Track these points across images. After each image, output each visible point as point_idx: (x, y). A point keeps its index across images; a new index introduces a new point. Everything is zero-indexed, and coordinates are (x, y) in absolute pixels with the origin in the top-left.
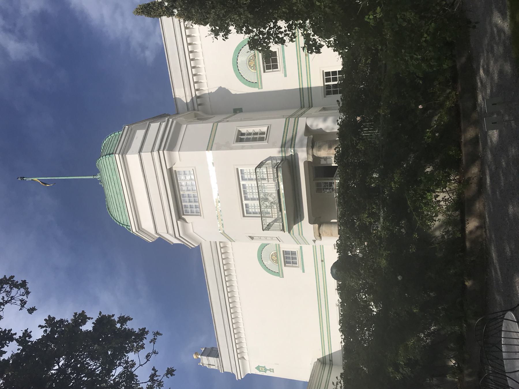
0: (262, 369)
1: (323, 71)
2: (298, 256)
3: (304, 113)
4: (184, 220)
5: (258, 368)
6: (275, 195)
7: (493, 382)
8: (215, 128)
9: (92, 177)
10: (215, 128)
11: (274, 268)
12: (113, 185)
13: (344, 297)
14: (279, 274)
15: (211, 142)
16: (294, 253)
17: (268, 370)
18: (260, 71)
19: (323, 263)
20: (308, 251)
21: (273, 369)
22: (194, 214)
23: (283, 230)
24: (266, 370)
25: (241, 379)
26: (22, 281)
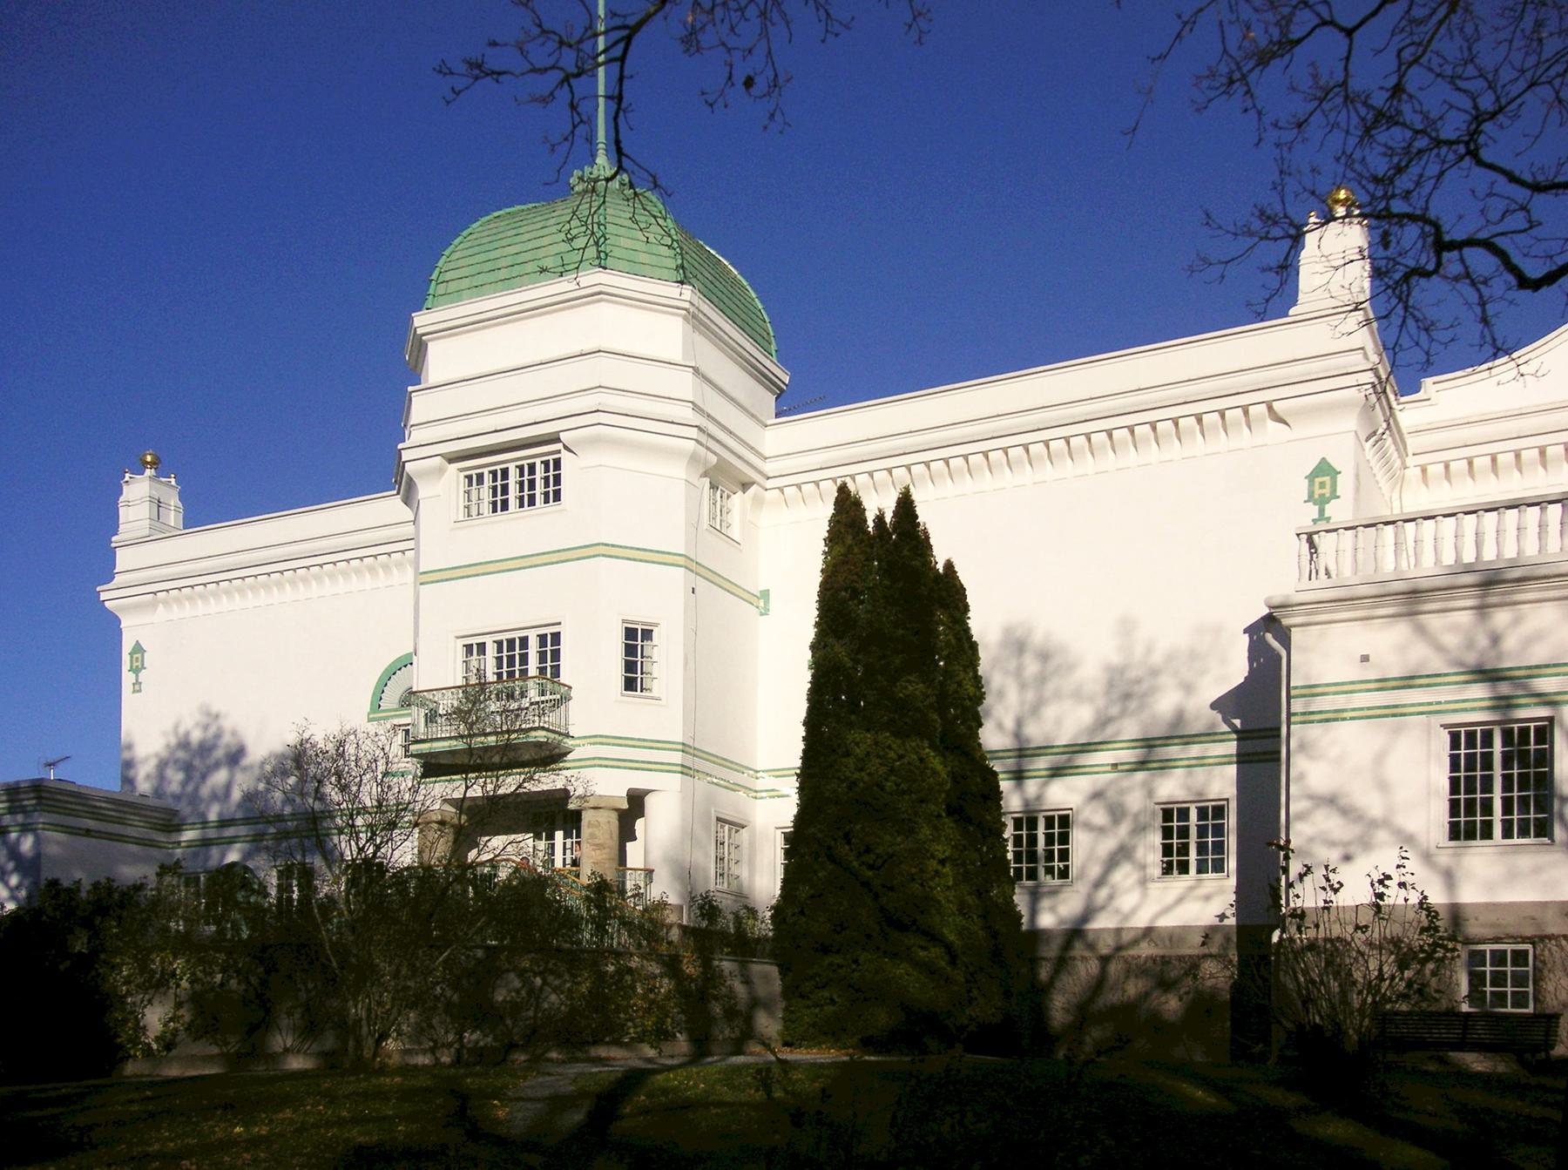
0: (1322, 485)
1: (656, 625)
3: (255, 820)
5: (138, 649)
13: (506, 927)
17: (137, 676)
19: (1109, 768)
21: (140, 691)
22: (1213, 803)
24: (136, 671)
25: (102, 599)
26: (906, 506)
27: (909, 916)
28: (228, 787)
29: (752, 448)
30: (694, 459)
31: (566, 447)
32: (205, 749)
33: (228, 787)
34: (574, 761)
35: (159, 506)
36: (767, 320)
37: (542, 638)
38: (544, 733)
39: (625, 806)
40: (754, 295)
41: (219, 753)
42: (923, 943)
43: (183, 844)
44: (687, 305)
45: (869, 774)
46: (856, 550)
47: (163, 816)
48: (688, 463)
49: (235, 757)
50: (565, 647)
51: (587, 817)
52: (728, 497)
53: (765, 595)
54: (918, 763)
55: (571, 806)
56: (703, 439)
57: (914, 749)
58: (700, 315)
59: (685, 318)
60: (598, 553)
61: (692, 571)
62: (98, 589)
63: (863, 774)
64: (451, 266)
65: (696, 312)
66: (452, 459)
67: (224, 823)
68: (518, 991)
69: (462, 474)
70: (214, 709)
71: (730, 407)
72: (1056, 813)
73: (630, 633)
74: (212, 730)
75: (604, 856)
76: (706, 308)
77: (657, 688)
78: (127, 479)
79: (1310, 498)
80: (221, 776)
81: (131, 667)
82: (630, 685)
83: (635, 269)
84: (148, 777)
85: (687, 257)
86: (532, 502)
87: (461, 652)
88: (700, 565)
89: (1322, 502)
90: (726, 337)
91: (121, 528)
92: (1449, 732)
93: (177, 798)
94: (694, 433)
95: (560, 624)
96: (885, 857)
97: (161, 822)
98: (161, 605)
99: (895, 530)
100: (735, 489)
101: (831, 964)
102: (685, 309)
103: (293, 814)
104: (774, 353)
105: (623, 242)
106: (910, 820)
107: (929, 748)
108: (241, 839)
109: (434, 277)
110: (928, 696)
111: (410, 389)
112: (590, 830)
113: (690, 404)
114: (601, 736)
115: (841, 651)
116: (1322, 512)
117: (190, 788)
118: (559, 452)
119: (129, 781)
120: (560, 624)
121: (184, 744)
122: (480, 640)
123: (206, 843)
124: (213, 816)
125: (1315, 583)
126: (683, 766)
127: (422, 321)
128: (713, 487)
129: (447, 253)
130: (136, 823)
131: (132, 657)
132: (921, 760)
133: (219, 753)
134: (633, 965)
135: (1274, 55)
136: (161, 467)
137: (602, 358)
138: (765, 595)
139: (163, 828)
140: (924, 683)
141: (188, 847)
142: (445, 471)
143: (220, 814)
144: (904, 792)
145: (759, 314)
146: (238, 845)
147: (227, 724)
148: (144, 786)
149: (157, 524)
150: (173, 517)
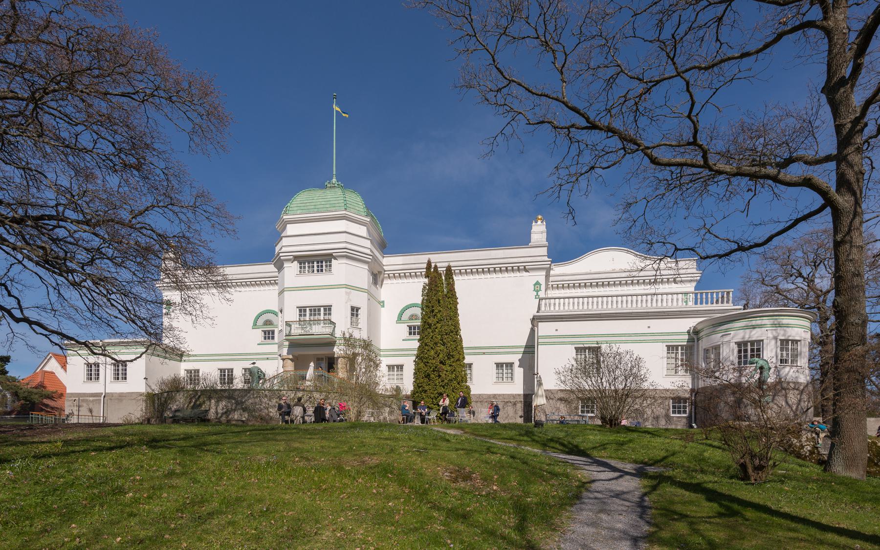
0: (537, 287)
2: (270, 341)
4: (294, 261)
6: (311, 332)
7: (115, 288)
8: (363, 290)
9: (334, 173)
10: (363, 290)
11: (261, 322)
12: (323, 203)
14: (255, 325)
15: (352, 288)
16: (273, 338)
18: (409, 323)
20: (274, 348)
23: (286, 336)
53: (383, 302)
72: (761, 353)
79: (534, 290)
86: (322, 271)
89: (537, 291)
92: (575, 348)
116: (537, 294)
125: (697, 306)
135: (813, 162)
138: (383, 302)
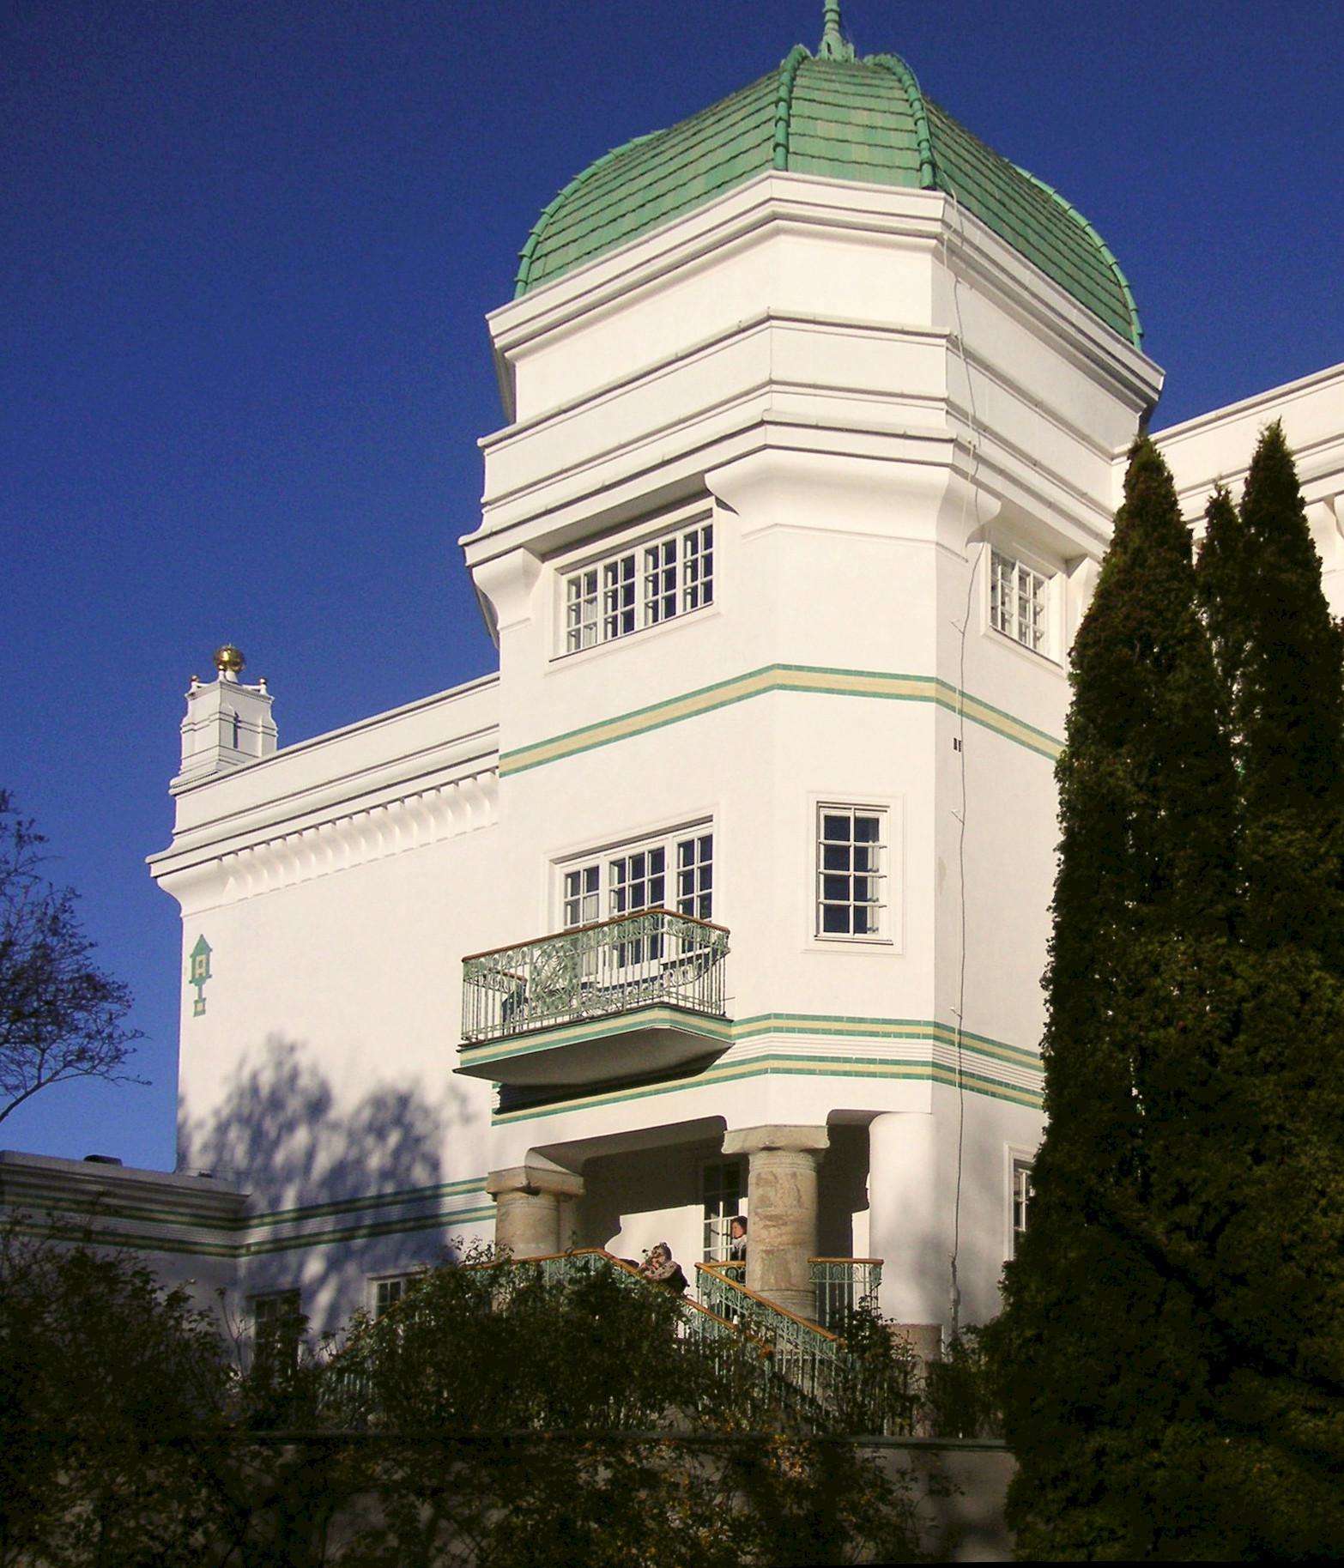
1: (883, 809)
5: (203, 948)
17: (200, 989)
21: (203, 1012)
24: (199, 981)
27: (1282, 1342)
28: (311, 1154)
29: (1083, 495)
30: (950, 503)
31: (721, 504)
32: (276, 1103)
33: (311, 1154)
34: (733, 1064)
35: (236, 727)
36: (1124, 282)
37: (687, 847)
38: (665, 1014)
39: (824, 1143)
40: (1098, 241)
41: (294, 1104)
42: (1317, 1403)
43: (253, 1249)
44: (936, 228)
45: (1184, 1030)
46: (1152, 560)
47: (223, 1205)
48: (942, 510)
49: (318, 1106)
50: (718, 862)
51: (757, 1165)
52: (1038, 584)
54: (1296, 1002)
55: (727, 1148)
56: (968, 465)
57: (1284, 970)
58: (966, 248)
59: (936, 254)
60: (771, 683)
61: (953, 709)
62: (148, 860)
63: (1171, 1030)
64: (554, 229)
65: (958, 241)
66: (548, 549)
67: (305, 1212)
68: (377, 1536)
69: (564, 579)
70: (290, 1036)
71: (1034, 419)
73: (835, 826)
74: (287, 1069)
75: (785, 1238)
76: (977, 234)
77: (884, 919)
78: (194, 689)
80: (301, 1136)
81: (193, 976)
82: (835, 920)
83: (839, 165)
84: (205, 1147)
85: (940, 145)
87: (560, 886)
88: (972, 699)
90: (1026, 295)
91: (185, 764)
93: (241, 1176)
94: (946, 453)
95: (709, 819)
96: (1225, 1211)
97: (223, 1215)
98: (231, 879)
99: (1248, 522)
100: (1051, 568)
101: (1100, 1453)
102: (935, 237)
103: (396, 1194)
104: (1136, 339)
105: (821, 128)
106: (1281, 1128)
107: (1322, 967)
108: (326, 1237)
109: (526, 251)
110: (1322, 859)
111: (481, 442)
112: (760, 1191)
113: (943, 405)
114: (777, 1016)
115: (1122, 766)
117: (259, 1162)
118: (708, 514)
119: (182, 1158)
120: (709, 819)
121: (255, 1090)
122: (589, 862)
123: (278, 1246)
124: (289, 1202)
126: (935, 1065)
127: (502, 323)
128: (1001, 561)
129: (550, 209)
130: (162, 1216)
131: (194, 961)
132: (1305, 996)
133: (294, 1104)
134: (654, 1463)
136: (245, 669)
137: (776, 331)
139: (230, 1225)
140: (1310, 830)
141: (258, 1253)
142: (536, 576)
143: (300, 1198)
144: (1267, 1068)
145: (1109, 274)
146: (322, 1248)
147: (303, 1059)
148: (199, 1161)
149: (233, 754)
150: (259, 743)
